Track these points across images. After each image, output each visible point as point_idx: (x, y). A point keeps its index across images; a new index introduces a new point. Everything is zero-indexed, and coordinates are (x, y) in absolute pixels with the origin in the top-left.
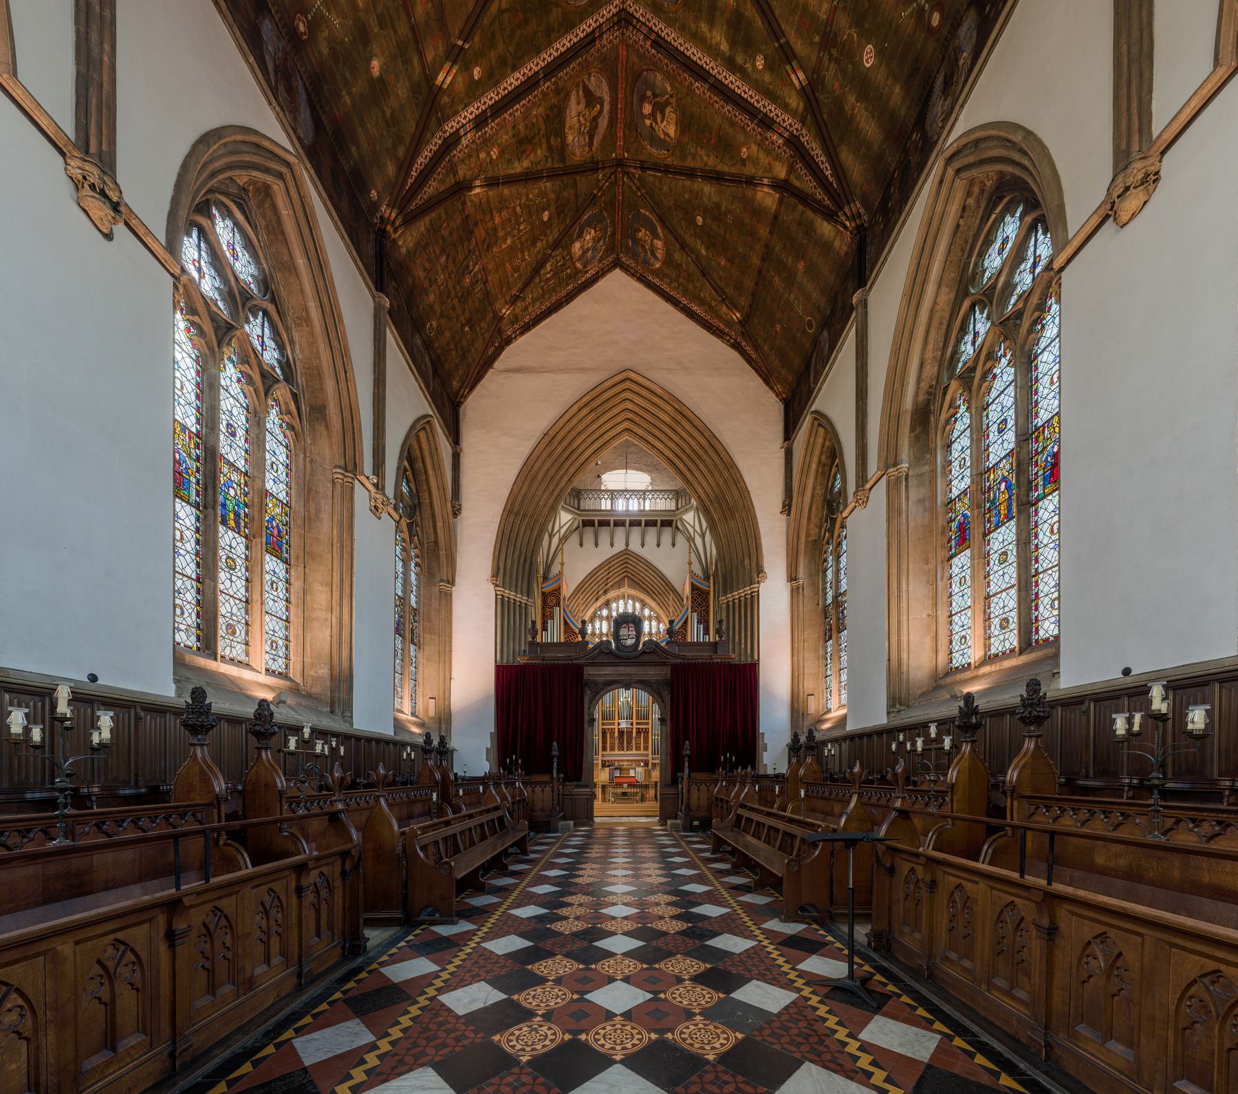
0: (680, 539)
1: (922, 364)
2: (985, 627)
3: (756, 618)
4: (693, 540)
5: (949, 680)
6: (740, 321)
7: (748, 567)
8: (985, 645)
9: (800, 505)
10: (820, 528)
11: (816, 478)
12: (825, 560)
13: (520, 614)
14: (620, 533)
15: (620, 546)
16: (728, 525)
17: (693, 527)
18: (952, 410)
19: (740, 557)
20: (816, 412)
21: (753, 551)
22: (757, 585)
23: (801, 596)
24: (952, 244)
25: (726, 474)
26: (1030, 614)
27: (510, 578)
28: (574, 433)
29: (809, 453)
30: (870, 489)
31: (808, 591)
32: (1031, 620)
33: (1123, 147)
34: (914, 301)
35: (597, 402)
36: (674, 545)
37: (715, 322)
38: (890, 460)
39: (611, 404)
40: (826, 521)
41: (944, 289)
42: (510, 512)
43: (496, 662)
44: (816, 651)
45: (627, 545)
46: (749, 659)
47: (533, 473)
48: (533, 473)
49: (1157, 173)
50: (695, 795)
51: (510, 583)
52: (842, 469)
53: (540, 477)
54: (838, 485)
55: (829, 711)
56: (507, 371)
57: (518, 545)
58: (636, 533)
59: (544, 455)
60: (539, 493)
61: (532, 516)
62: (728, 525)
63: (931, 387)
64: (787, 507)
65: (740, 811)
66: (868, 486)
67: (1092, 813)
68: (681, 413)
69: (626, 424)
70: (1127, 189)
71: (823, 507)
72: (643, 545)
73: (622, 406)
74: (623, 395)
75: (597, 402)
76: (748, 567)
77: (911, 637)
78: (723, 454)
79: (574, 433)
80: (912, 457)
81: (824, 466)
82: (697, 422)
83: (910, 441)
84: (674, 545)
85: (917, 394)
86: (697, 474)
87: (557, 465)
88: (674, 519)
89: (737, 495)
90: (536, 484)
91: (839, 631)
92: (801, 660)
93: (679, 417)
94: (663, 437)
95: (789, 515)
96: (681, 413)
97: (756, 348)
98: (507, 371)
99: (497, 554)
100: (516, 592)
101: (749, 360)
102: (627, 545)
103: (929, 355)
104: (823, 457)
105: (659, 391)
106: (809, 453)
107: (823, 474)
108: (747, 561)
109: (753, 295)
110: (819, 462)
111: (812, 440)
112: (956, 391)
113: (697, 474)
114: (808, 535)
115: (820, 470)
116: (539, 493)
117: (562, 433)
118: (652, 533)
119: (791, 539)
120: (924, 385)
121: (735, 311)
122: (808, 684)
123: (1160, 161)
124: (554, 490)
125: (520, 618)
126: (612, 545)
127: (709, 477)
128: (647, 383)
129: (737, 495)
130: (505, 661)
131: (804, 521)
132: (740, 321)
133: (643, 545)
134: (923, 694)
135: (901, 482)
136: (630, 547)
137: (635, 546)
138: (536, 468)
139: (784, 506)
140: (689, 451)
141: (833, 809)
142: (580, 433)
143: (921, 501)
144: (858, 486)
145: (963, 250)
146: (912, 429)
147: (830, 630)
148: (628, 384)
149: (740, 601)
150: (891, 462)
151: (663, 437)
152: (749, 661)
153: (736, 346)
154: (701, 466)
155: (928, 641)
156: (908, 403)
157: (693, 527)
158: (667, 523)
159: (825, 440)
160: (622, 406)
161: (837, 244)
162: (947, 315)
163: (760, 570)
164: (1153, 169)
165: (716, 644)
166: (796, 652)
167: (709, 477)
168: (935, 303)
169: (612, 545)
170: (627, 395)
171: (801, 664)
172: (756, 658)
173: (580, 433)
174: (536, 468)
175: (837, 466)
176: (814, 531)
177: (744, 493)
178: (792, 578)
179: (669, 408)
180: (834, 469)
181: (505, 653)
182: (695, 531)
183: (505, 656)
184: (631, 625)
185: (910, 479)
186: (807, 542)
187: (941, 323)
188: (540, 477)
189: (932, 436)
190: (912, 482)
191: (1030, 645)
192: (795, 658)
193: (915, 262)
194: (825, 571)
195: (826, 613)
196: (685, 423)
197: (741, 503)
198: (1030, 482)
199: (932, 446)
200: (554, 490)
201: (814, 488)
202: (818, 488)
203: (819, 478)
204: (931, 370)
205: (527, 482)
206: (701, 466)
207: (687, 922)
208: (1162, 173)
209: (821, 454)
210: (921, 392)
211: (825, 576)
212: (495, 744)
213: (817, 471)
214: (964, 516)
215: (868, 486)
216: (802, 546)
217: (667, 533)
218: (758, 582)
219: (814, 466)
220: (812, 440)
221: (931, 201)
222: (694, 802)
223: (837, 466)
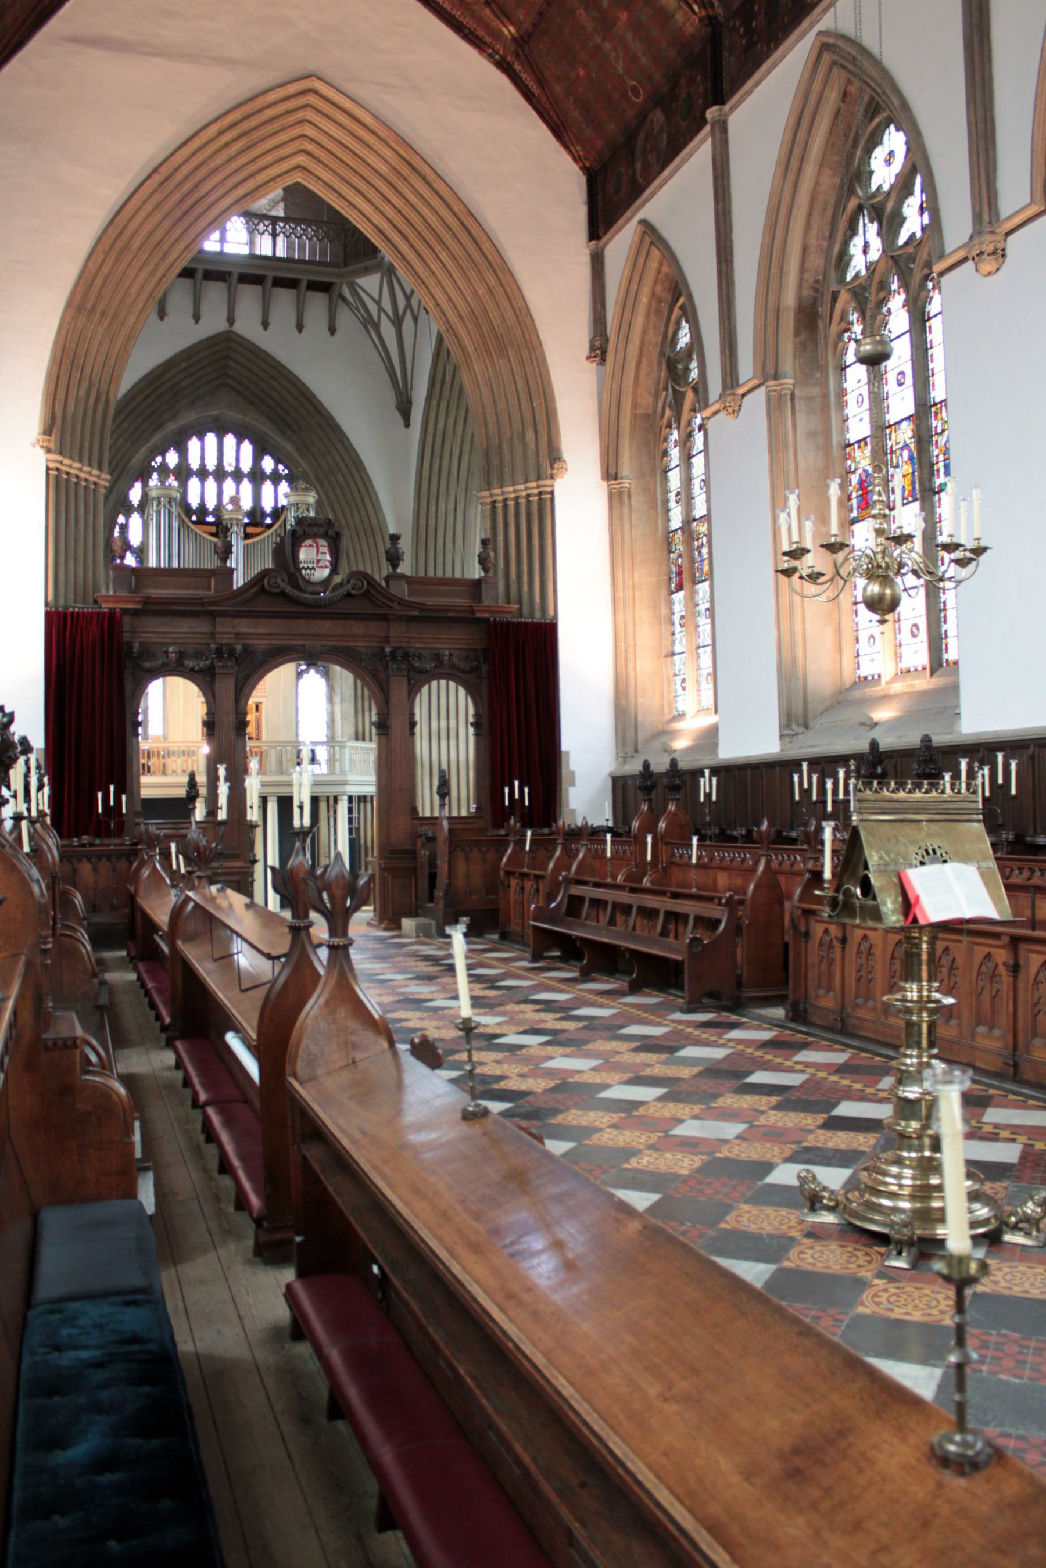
0: (346, 319)
1: (805, 250)
2: (895, 630)
3: (549, 541)
4: (377, 326)
5: (857, 694)
6: (514, 39)
7: (532, 446)
8: (896, 653)
9: (621, 354)
10: (657, 396)
11: (648, 317)
12: (665, 453)
13: (86, 504)
14: (215, 294)
15: (213, 323)
16: (493, 363)
17: (378, 303)
18: (843, 325)
19: (517, 426)
20: (644, 222)
21: (541, 419)
22: (548, 482)
23: (626, 509)
24: (834, 124)
25: (492, 281)
26: (939, 627)
27: (72, 435)
28: (204, 171)
29: (636, 278)
30: (743, 396)
31: (638, 501)
32: (940, 634)
33: (978, 211)
34: (791, 176)
35: (254, 122)
36: (332, 330)
37: (468, 22)
38: (768, 372)
39: (276, 125)
40: (666, 389)
41: (827, 171)
42: (80, 309)
43: (47, 604)
44: (656, 607)
45: (231, 320)
46: (538, 614)
47: (124, 238)
48: (124, 238)
49: (1003, 250)
50: (462, 868)
51: (72, 448)
52: (690, 314)
53: (136, 244)
54: (684, 338)
55: (681, 716)
56: (75, 40)
57: (88, 371)
58: (249, 298)
59: (149, 207)
60: (131, 273)
61: (115, 315)
62: (493, 363)
63: (817, 282)
64: (599, 351)
65: (576, 890)
66: (740, 391)
67: (1032, 871)
68: (409, 164)
69: (301, 159)
70: (981, 253)
71: (660, 364)
72: (265, 325)
73: (296, 131)
74: (300, 115)
75: (254, 122)
76: (532, 446)
77: (808, 627)
78: (486, 246)
79: (204, 171)
80: (798, 371)
81: (660, 301)
82: (439, 185)
83: (795, 349)
84: (332, 330)
85: (800, 286)
86: (435, 266)
87: (167, 224)
88: (337, 281)
89: (509, 314)
90: (128, 257)
91: (695, 582)
92: (630, 621)
93: (406, 171)
94: (371, 194)
95: (603, 360)
96: (409, 164)
97: (541, 82)
98: (75, 40)
99: (52, 388)
100: (100, 469)
101: (527, 95)
102: (231, 320)
103: (813, 241)
104: (659, 289)
105: (368, 120)
106: (636, 278)
107: (658, 312)
108: (530, 436)
109: (541, 14)
110: (653, 294)
111: (641, 261)
112: (847, 303)
113: (435, 266)
114: (635, 405)
115: (654, 306)
116: (131, 273)
117: (184, 171)
118: (284, 300)
119: (606, 407)
120: (810, 277)
121: (508, 24)
122: (644, 665)
123: (1005, 240)
124: (157, 266)
125: (86, 512)
126: (197, 318)
127: (456, 274)
128: (348, 105)
129: (509, 314)
130: (62, 602)
131: (629, 383)
132: (514, 39)
133: (265, 325)
134: (826, 710)
135: (785, 401)
136: (239, 328)
137: (248, 326)
138: (132, 227)
139: (592, 348)
140: (421, 228)
141: (715, 883)
142: (216, 170)
143: (811, 435)
144: (725, 387)
145: (846, 136)
146: (797, 333)
147: (680, 573)
148: (311, 99)
149: (517, 504)
150: (771, 371)
151: (371, 194)
152: (538, 617)
153: (504, 66)
154: (443, 256)
155: (829, 633)
156: (790, 299)
157: (378, 303)
158: (325, 288)
159: (661, 264)
160: (296, 131)
161: (679, 17)
162: (832, 201)
163: (555, 457)
164: (1000, 246)
165: (478, 583)
166: (620, 607)
167: (456, 274)
168: (817, 183)
169: (197, 318)
170: (309, 114)
171: (630, 629)
172: (551, 613)
173: (216, 170)
174: (132, 227)
175: (682, 308)
176: (645, 400)
177: (524, 318)
178: (610, 474)
179: (387, 153)
180: (676, 312)
181: (62, 585)
182: (381, 309)
183: (62, 592)
184: (322, 542)
185: (797, 401)
186: (634, 416)
187: (825, 209)
188: (136, 244)
189: (821, 347)
190: (800, 405)
191: (941, 665)
192: (620, 617)
193: (790, 132)
194: (666, 471)
195: (669, 544)
196: (414, 180)
197: (519, 333)
198: (932, 465)
199: (822, 362)
200: (157, 266)
201: (644, 332)
202: (651, 332)
203: (653, 317)
204: (816, 261)
205: (113, 256)
206: (443, 256)
207: (526, 1065)
208: (1008, 252)
209: (656, 283)
210: (805, 285)
211: (665, 480)
212: (135, 780)
213: (649, 307)
214: (865, 471)
215: (740, 391)
216: (626, 423)
217: (317, 305)
218: (552, 477)
219: (644, 300)
220: (641, 261)
221: (807, 75)
222: (460, 881)
223: (682, 308)
